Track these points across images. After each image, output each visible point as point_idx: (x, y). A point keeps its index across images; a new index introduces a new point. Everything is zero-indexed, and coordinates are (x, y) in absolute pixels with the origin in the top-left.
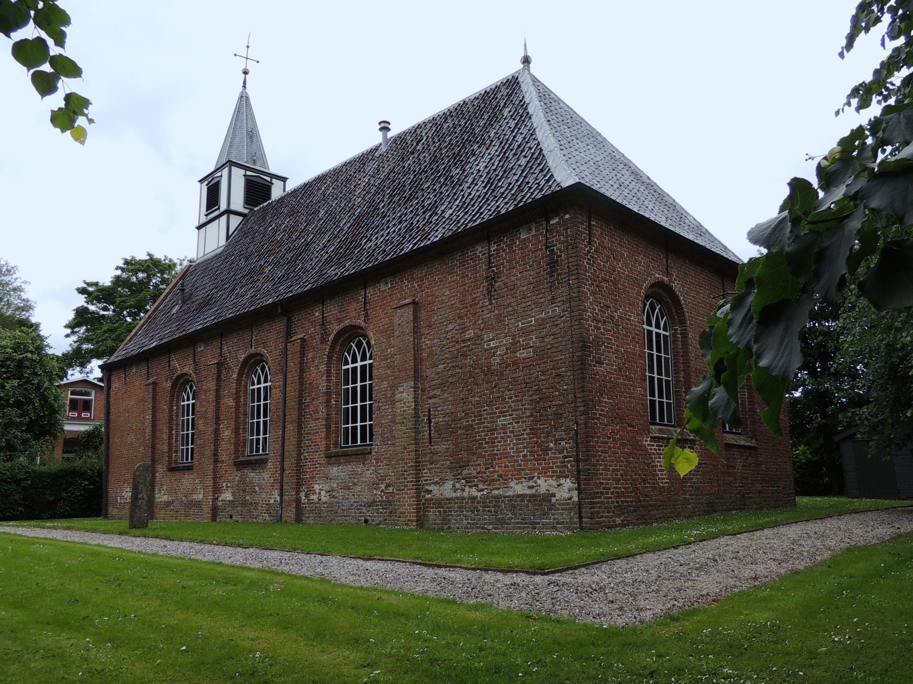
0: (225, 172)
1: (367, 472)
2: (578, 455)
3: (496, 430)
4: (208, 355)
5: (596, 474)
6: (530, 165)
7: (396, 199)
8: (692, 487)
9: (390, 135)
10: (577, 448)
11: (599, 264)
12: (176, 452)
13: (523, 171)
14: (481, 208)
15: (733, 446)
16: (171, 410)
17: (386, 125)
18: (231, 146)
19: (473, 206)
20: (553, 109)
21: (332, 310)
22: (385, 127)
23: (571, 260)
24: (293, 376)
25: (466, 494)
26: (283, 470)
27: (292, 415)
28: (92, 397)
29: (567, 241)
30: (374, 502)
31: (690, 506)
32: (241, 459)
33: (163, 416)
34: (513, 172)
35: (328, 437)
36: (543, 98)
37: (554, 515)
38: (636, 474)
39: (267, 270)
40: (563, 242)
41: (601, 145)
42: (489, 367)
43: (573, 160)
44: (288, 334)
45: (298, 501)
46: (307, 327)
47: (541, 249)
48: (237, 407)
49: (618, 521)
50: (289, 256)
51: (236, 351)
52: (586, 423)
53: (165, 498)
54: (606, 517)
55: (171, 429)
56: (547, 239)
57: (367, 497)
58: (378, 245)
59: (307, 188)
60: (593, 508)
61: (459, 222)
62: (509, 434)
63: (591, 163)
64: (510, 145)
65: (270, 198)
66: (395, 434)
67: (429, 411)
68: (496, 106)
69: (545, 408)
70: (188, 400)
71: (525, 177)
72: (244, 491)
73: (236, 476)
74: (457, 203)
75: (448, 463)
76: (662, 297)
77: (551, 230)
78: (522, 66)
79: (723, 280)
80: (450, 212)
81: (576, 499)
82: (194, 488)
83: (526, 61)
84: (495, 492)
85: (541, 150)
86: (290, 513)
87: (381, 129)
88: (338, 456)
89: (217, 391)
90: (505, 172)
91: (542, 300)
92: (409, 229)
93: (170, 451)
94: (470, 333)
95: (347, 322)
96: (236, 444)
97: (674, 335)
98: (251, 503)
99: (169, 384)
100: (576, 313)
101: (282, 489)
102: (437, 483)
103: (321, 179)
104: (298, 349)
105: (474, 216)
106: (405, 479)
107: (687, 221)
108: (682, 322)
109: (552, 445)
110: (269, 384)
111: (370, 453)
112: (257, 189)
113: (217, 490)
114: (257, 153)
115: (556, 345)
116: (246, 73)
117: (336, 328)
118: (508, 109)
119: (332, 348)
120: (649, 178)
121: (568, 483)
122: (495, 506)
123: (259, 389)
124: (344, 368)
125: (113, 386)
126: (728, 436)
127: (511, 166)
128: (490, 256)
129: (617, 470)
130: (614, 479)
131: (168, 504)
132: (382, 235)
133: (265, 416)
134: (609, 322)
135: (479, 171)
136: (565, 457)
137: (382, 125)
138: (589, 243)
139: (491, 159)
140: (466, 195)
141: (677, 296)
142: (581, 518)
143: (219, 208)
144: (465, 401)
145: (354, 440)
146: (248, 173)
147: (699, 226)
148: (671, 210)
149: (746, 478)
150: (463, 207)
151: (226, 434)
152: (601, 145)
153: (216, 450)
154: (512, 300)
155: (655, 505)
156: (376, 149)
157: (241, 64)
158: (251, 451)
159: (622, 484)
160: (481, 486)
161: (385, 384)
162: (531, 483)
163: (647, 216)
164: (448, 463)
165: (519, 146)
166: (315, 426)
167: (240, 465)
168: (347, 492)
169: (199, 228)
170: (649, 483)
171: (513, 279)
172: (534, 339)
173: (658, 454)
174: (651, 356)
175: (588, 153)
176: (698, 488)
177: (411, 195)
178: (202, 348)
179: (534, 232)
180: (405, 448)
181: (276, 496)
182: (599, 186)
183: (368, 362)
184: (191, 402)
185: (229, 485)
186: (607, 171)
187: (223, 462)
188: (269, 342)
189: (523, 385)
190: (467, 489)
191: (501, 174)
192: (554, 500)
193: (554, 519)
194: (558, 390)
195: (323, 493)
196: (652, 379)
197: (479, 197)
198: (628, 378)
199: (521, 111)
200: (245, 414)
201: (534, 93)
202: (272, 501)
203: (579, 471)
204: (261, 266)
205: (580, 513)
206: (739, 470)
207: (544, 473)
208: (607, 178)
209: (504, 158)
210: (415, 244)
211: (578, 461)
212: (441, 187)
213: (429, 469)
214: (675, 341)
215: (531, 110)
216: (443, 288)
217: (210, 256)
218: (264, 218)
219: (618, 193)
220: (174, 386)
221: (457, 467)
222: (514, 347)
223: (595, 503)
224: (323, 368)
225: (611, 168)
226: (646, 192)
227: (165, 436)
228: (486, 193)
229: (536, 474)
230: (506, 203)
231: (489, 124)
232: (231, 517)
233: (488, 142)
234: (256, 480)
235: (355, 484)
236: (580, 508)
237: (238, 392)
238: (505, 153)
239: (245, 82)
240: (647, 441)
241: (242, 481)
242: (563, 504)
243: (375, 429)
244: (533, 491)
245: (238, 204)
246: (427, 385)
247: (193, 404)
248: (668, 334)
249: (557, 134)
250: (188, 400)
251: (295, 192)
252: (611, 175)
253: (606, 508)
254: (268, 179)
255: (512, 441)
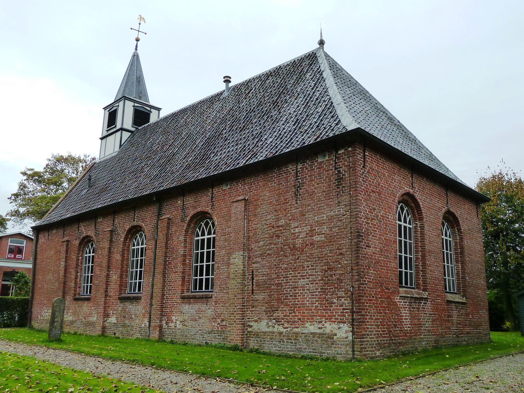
0: (121, 104)
1: (208, 310)
2: (353, 309)
3: (297, 287)
4: (105, 225)
5: (364, 322)
6: (324, 112)
7: (234, 128)
8: (425, 330)
9: (230, 85)
10: (353, 303)
11: (370, 181)
12: (80, 287)
13: (320, 116)
14: (292, 139)
15: (451, 302)
16: (78, 260)
17: (228, 79)
18: (125, 87)
19: (286, 137)
20: (338, 75)
21: (190, 200)
22: (227, 80)
23: (351, 178)
24: (161, 243)
25: (275, 330)
26: (151, 305)
27: (159, 269)
28: (24, 245)
29: (349, 165)
30: (212, 331)
31: (423, 343)
32: (123, 295)
33: (73, 263)
34: (313, 116)
35: (183, 285)
36: (332, 67)
37: (335, 348)
38: (390, 322)
39: (146, 170)
40: (347, 166)
41: (368, 100)
42: (294, 244)
43: (352, 111)
44: (159, 215)
45: (161, 327)
46: (173, 210)
47: (332, 170)
48: (122, 261)
49: (378, 353)
50: (161, 162)
51: (123, 223)
52: (359, 287)
53: (70, 318)
54: (370, 351)
55: (77, 272)
56: (336, 163)
57: (208, 327)
58: (223, 160)
59: (175, 116)
60: (362, 345)
61: (277, 147)
62: (306, 291)
63: (363, 112)
64: (311, 98)
65: (148, 121)
66: (228, 285)
67: (253, 272)
68: (301, 71)
69: (331, 276)
70: (90, 253)
71: (321, 120)
72: (124, 317)
73: (120, 306)
74: (275, 134)
75: (264, 308)
76: (409, 202)
77: (339, 157)
78: (319, 46)
79: (365, 147)
80: (271, 140)
81: (350, 338)
82: (91, 313)
83: (322, 43)
84: (296, 330)
85: (332, 103)
86: (155, 335)
87: (225, 81)
88: (189, 298)
89: (110, 248)
90: (307, 116)
91: (332, 203)
92: (243, 149)
93: (75, 287)
94: (282, 222)
95: (199, 209)
96: (121, 285)
97: (415, 228)
98: (129, 326)
99: (77, 242)
100: (354, 213)
101: (150, 318)
102: (256, 321)
103: (184, 111)
104: (166, 225)
105: (287, 144)
106: (235, 317)
107: (423, 151)
108: (421, 219)
109: (335, 301)
110: (144, 246)
111: (211, 297)
112: (141, 116)
113: (106, 315)
114: (142, 92)
115: (339, 234)
116: (137, 40)
117: (191, 212)
118: (310, 74)
119: (189, 225)
120: (399, 122)
121: (346, 327)
122: (295, 339)
123: (89, 257)
124: (196, 239)
125: (40, 241)
126: (448, 295)
127: (311, 112)
128: (297, 172)
129: (378, 319)
130: (376, 325)
131: (72, 322)
132: (225, 152)
133: (141, 267)
134: (374, 219)
135: (290, 114)
136: (344, 309)
137: (226, 79)
138: (364, 167)
139: (298, 106)
140: (281, 129)
141: (418, 202)
142: (353, 351)
143: (116, 127)
144: (277, 267)
145: (201, 288)
146: (136, 105)
147: (431, 155)
148: (413, 143)
149: (460, 324)
150: (280, 137)
151: (114, 278)
152: (368, 100)
153: (107, 288)
154: (311, 202)
155: (401, 343)
156: (221, 93)
157: (135, 34)
158: (131, 290)
159: (381, 328)
160: (286, 325)
161: (223, 252)
162: (320, 326)
163: (400, 149)
164: (264, 308)
165: (317, 99)
166: (175, 278)
167: (123, 299)
168: (194, 323)
169: (102, 139)
170: (398, 327)
171: (312, 187)
172: (325, 229)
173: (404, 308)
174: (400, 241)
175: (361, 104)
176: (429, 331)
177: (244, 126)
178: (101, 220)
179: (327, 158)
180: (235, 296)
181: (146, 322)
182: (369, 128)
183: (212, 236)
184: (91, 255)
185: (114, 312)
186: (373, 118)
187: (110, 297)
188: (146, 218)
189: (317, 259)
190: (276, 326)
191: (305, 117)
192: (335, 337)
193: (335, 351)
194: (340, 263)
195: (178, 322)
196: (400, 257)
197: (290, 131)
198: (387, 257)
199: (318, 76)
200: (127, 265)
201: (327, 64)
202: (143, 325)
203: (353, 320)
204: (142, 167)
205: (353, 348)
206: (455, 318)
207: (329, 319)
208: (374, 122)
209: (307, 106)
210: (247, 160)
211: (353, 312)
212: (264, 123)
213: (251, 311)
214: (416, 232)
215: (325, 75)
216: (265, 191)
217: (108, 157)
218: (145, 134)
219: (380, 133)
220: (80, 244)
221: (271, 311)
222: (312, 233)
223: (363, 342)
224: (182, 238)
225: (376, 115)
226: (397, 131)
227: (73, 277)
228: (295, 129)
229: (324, 319)
230: (309, 137)
231: (297, 82)
232: (115, 334)
233: (296, 95)
234: (133, 311)
235: (200, 318)
236: (353, 345)
237: (123, 250)
238: (308, 103)
239: (137, 46)
240: (397, 299)
241: (124, 310)
242: (341, 341)
243: (216, 282)
244: (321, 331)
245: (128, 123)
246: (252, 254)
247: (93, 256)
248: (411, 226)
249: (342, 92)
250: (90, 253)
251: (166, 118)
252: (375, 120)
253: (370, 345)
254: (149, 109)
255: (308, 296)
